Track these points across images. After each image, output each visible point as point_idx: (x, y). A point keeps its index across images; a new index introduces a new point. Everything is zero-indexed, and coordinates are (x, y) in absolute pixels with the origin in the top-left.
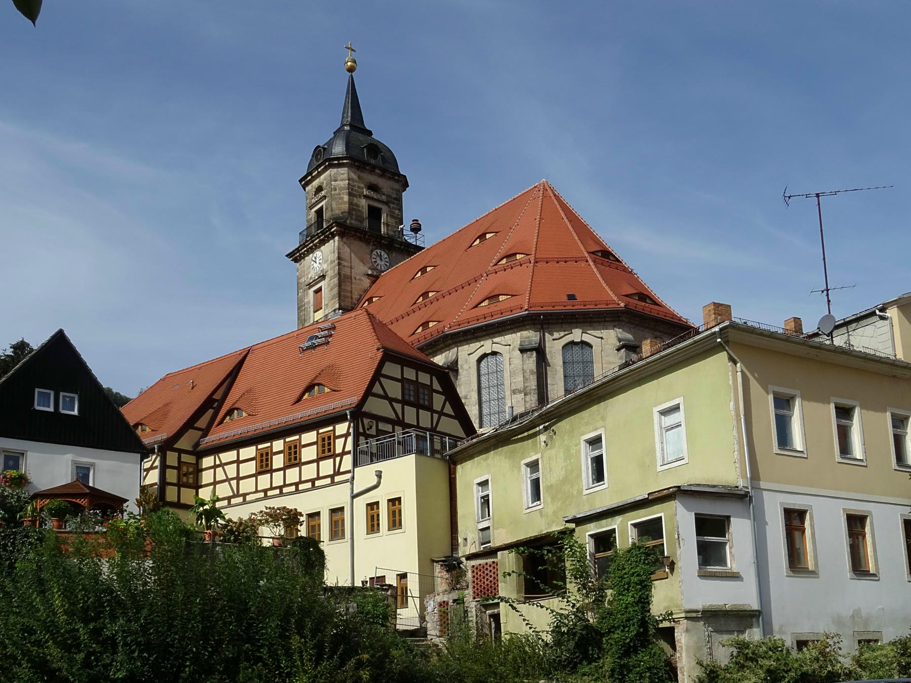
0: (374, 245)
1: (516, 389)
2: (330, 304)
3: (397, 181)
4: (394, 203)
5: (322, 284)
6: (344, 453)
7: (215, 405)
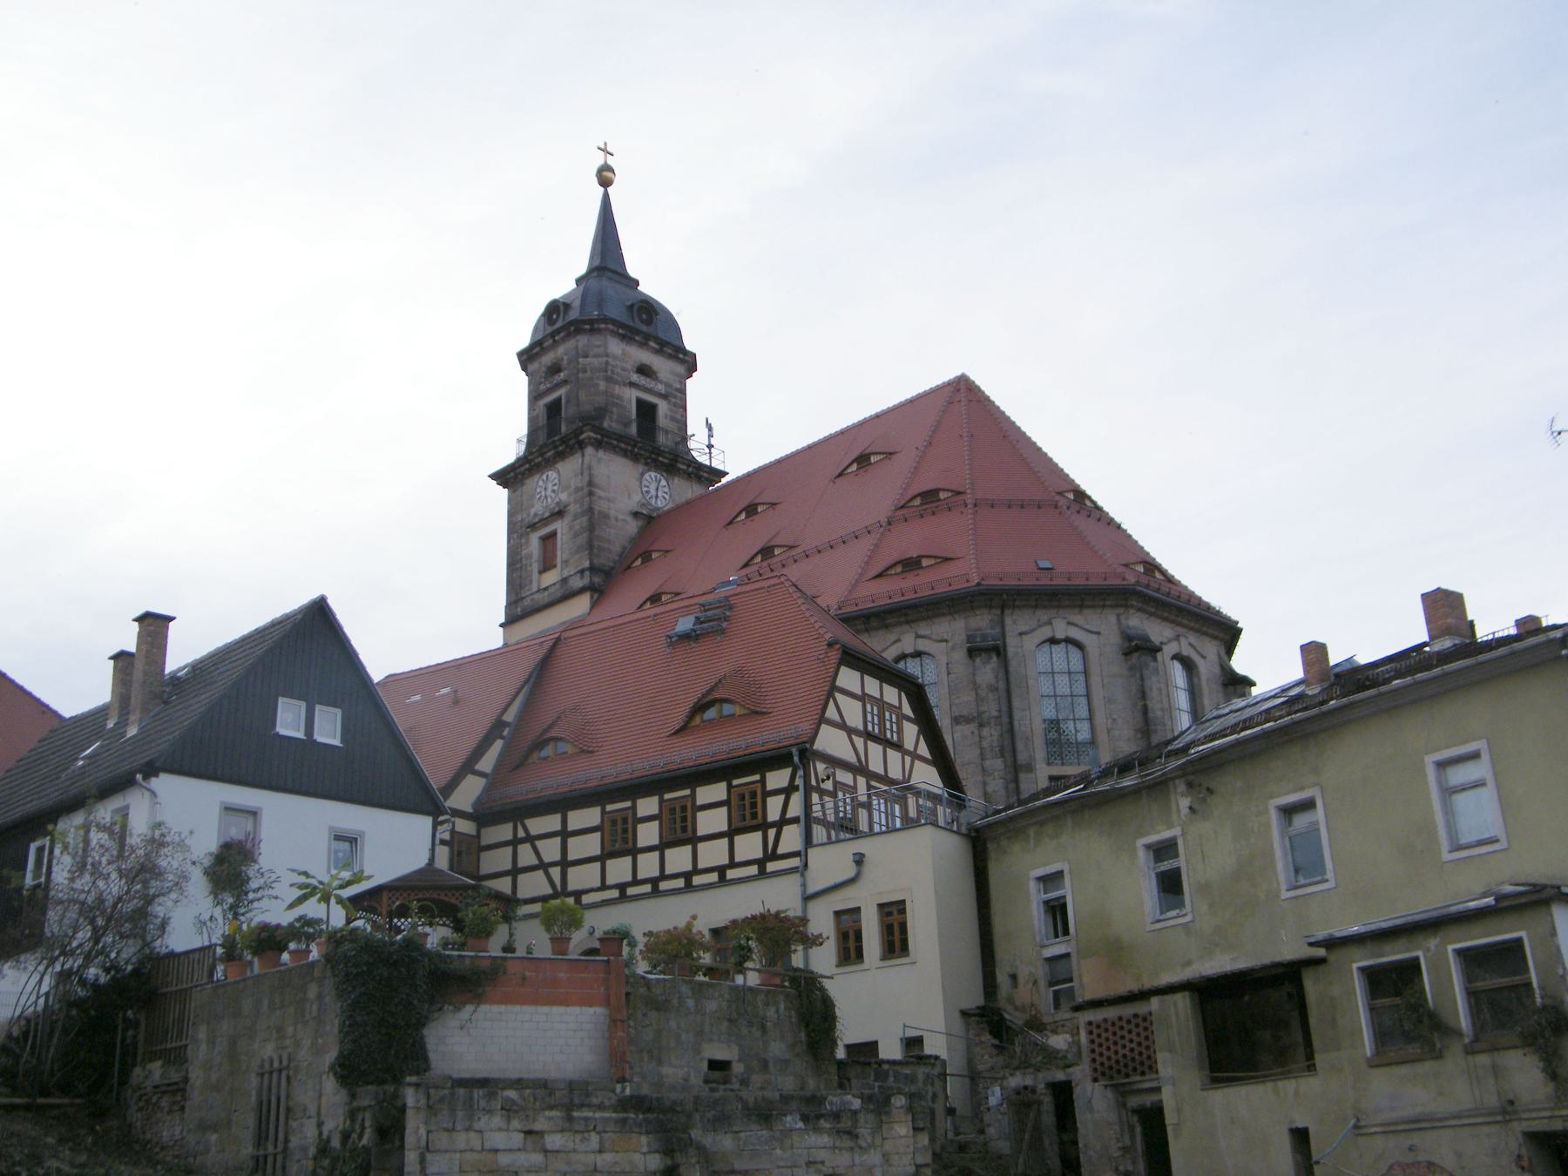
0: (647, 464)
1: (961, 716)
2: (572, 561)
3: (682, 362)
4: (675, 397)
5: (559, 526)
6: (783, 821)
7: (505, 733)
